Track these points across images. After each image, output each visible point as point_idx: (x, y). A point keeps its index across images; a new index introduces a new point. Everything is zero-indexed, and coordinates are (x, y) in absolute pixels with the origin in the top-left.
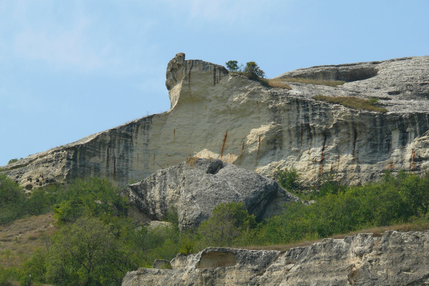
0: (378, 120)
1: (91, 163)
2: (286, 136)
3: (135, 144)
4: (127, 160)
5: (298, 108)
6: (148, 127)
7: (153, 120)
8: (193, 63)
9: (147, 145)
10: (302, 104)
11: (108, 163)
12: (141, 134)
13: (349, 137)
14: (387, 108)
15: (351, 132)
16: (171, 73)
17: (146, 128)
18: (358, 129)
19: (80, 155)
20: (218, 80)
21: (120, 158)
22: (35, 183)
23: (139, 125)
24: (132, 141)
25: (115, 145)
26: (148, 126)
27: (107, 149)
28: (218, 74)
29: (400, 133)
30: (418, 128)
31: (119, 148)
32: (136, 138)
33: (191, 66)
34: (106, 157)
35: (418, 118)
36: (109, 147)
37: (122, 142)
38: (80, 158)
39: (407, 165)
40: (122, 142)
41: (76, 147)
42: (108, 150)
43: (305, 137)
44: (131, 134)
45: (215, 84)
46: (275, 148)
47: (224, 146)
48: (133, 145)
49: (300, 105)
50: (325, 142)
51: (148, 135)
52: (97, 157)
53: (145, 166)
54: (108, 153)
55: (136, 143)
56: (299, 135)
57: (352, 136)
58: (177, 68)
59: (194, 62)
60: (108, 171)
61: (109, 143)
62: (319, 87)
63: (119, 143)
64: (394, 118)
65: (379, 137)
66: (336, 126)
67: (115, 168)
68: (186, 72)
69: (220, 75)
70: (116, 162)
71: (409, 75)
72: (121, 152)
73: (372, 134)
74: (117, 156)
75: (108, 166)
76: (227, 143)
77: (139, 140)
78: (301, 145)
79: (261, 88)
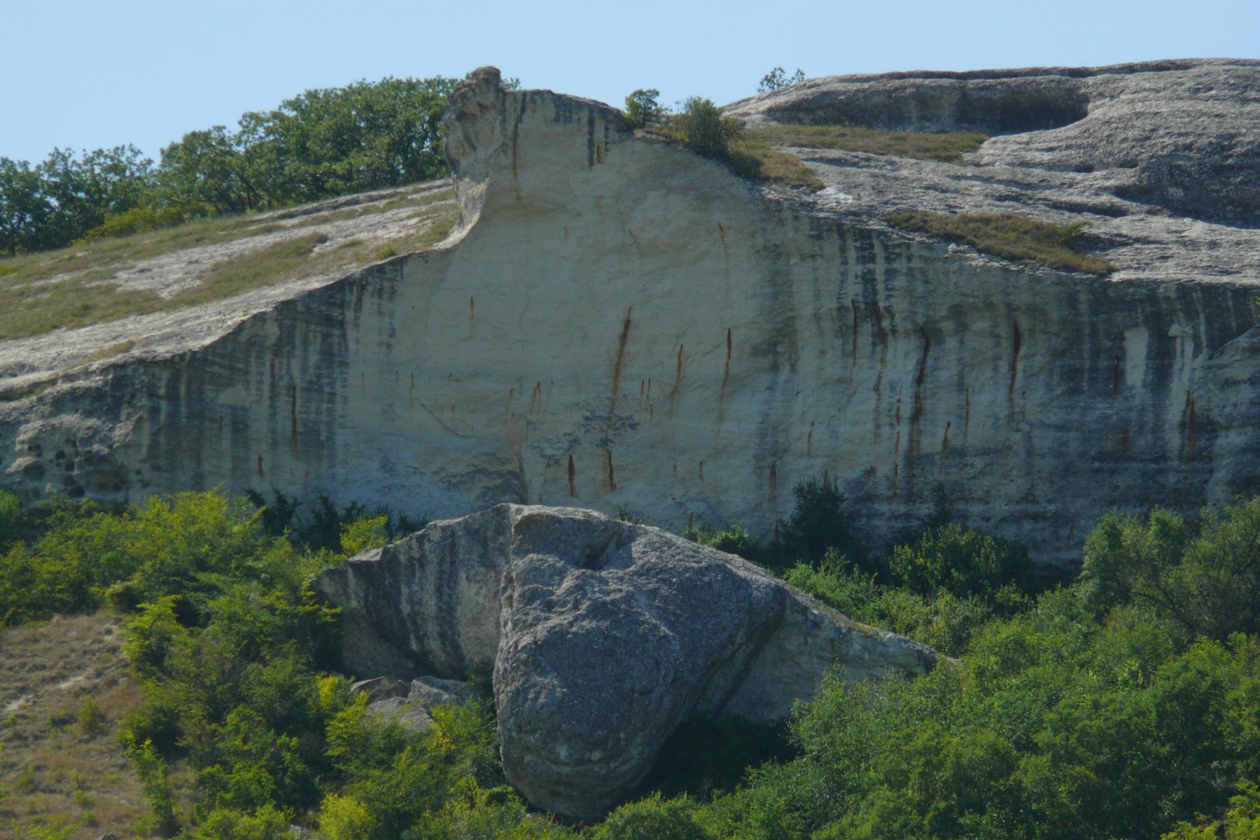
0: (1083, 297)
1: (222, 406)
2: (806, 329)
3: (352, 346)
4: (332, 394)
5: (843, 249)
6: (393, 291)
7: (407, 269)
8: (524, 100)
9: (389, 346)
10: (855, 240)
11: (273, 406)
12: (372, 294)
13: (998, 344)
14: (1111, 254)
15: (1004, 331)
16: (457, 124)
17: (386, 296)
18: (1024, 323)
19: (189, 382)
20: (602, 151)
21: (309, 390)
22: (51, 461)
23: (363, 288)
24: (343, 336)
25: (294, 348)
26: (392, 288)
27: (268, 364)
28: (599, 135)
29: (1150, 336)
30: (1203, 328)
31: (306, 358)
32: (357, 326)
33: (519, 111)
34: (266, 387)
35: (1203, 298)
36: (276, 355)
37: (315, 337)
38: (188, 394)
39: (1174, 440)
40: (315, 337)
41: (176, 359)
42: (273, 366)
43: (865, 340)
44: (342, 314)
45: (591, 164)
46: (775, 368)
47: (621, 354)
48: (346, 346)
49: (850, 243)
50: (925, 356)
51: (392, 315)
52: (240, 386)
53: (385, 412)
54: (273, 376)
55: (357, 341)
56: (847, 332)
57: (1005, 344)
58: (478, 113)
59: (528, 97)
60: (274, 431)
61: (275, 345)
62: (907, 168)
63: (305, 344)
64: (1133, 294)
65: (1086, 347)
66: (957, 312)
67: (294, 421)
68: (504, 130)
69: (606, 136)
70: (299, 401)
71: (1180, 135)
72: (311, 371)
73: (1067, 339)
74: (298, 383)
75: (273, 415)
76: (630, 348)
77: (364, 332)
78: (854, 364)
79: (732, 185)
